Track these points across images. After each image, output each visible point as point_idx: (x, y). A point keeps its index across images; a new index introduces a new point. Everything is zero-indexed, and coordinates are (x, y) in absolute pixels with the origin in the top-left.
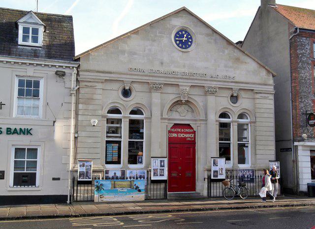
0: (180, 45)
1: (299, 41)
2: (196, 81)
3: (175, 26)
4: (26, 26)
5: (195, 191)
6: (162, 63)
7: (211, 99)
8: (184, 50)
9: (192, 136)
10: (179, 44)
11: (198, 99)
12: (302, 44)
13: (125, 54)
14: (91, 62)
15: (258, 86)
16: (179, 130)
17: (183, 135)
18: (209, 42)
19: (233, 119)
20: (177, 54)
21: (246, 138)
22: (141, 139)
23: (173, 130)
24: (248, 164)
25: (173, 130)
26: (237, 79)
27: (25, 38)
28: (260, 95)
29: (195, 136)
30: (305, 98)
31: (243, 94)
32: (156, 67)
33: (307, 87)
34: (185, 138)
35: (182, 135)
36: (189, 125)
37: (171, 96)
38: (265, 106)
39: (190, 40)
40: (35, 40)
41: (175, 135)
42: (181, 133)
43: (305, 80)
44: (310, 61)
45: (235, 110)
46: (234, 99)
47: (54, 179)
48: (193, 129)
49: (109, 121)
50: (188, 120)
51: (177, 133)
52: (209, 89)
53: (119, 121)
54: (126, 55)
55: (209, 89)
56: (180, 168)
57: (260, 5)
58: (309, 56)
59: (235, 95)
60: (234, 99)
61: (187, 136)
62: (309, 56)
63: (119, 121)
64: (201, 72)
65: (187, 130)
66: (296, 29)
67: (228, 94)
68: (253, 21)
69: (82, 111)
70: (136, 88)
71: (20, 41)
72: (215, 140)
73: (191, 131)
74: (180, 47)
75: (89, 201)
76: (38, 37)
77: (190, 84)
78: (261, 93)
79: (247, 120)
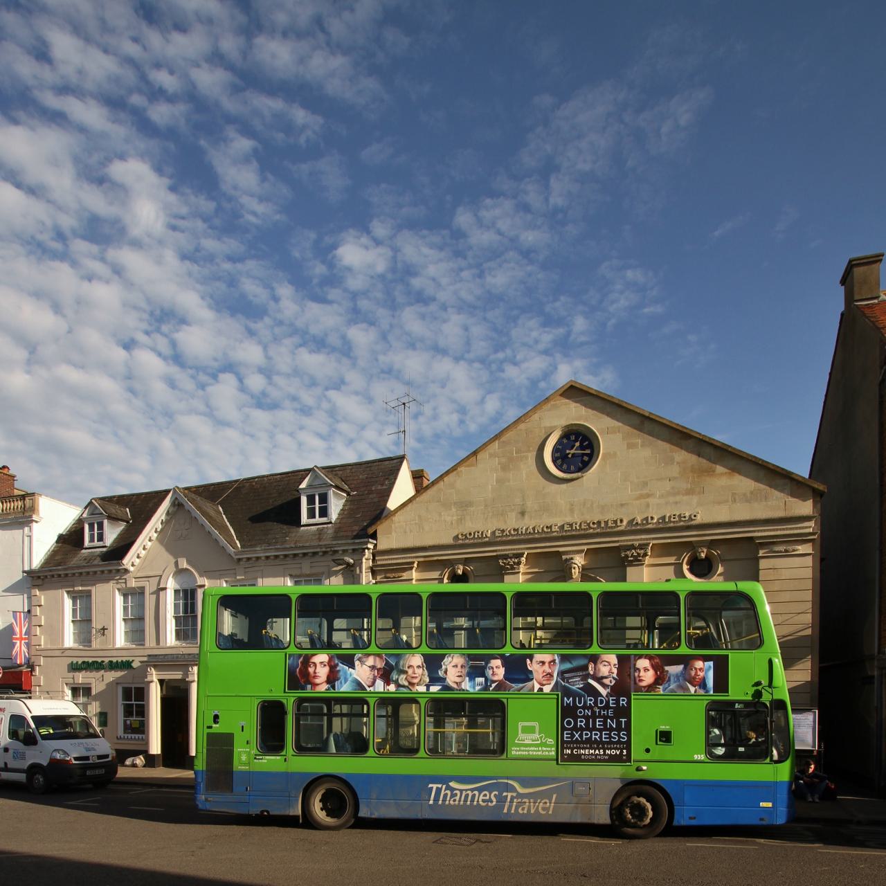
13: (451, 509)
18: (631, 446)
26: (699, 520)
27: (311, 514)
47: (243, 727)
54: (454, 510)
71: (304, 519)
74: (564, 472)
76: (308, 505)
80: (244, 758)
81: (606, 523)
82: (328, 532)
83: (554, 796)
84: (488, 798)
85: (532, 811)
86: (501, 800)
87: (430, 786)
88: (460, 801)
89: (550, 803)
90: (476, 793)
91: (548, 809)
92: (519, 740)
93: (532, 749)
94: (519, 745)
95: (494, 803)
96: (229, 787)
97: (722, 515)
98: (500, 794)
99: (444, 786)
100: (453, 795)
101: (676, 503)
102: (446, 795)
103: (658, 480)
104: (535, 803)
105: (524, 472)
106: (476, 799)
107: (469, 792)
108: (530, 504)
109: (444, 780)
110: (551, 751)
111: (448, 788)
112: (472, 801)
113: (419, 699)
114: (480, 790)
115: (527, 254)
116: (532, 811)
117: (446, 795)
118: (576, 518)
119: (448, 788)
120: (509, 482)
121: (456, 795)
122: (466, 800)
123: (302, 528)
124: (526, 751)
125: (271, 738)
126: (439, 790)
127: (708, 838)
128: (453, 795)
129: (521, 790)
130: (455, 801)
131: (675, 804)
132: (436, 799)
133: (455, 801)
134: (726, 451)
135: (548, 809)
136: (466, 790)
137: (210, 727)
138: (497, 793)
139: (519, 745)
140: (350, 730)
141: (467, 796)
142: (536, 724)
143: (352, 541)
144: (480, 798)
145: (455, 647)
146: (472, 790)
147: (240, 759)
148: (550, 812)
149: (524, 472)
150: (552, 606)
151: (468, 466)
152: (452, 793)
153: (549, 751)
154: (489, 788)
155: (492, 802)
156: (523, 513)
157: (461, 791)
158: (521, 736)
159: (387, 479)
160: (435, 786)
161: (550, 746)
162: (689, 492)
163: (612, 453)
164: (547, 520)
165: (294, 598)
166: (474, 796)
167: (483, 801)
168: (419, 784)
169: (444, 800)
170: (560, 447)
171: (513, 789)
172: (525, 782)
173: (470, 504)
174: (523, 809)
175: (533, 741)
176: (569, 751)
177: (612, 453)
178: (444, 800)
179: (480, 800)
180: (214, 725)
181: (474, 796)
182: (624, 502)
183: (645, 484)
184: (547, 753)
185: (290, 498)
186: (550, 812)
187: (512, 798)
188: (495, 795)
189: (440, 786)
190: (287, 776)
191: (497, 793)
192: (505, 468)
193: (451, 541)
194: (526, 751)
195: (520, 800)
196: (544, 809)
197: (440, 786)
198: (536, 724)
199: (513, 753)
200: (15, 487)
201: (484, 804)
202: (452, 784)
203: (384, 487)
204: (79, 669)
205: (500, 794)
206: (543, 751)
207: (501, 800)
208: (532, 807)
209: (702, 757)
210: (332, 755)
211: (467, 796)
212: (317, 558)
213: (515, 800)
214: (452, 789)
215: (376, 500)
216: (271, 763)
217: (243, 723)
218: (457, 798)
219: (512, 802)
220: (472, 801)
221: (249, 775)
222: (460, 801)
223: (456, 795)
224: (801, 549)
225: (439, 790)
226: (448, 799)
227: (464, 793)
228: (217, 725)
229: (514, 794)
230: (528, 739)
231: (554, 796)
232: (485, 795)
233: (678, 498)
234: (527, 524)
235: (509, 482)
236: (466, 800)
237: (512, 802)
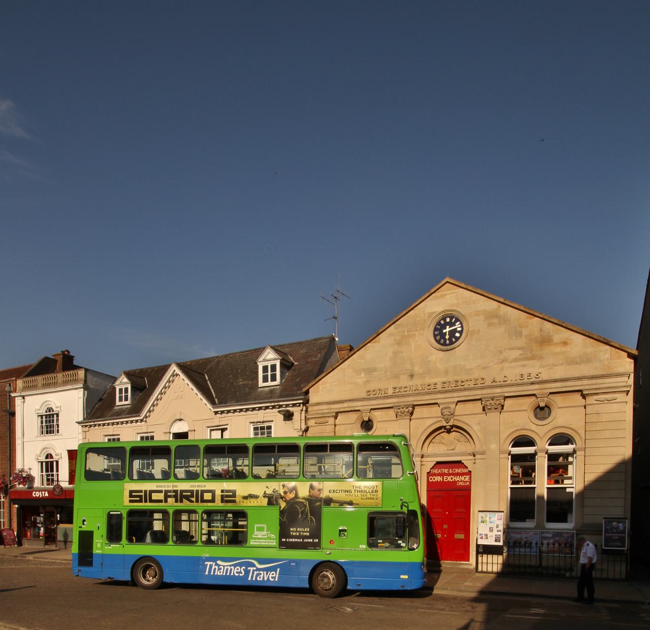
0: (438, 338)
2: (466, 393)
3: (446, 332)
4: (265, 364)
5: (469, 561)
6: (412, 376)
8: (449, 347)
9: (467, 479)
11: (470, 416)
16: (446, 471)
17: (452, 478)
18: (489, 325)
19: (543, 449)
20: (437, 357)
21: (570, 478)
22: (210, 530)
23: (436, 471)
24: (572, 522)
25: (436, 471)
26: (544, 377)
28: (595, 397)
29: (470, 478)
31: (558, 400)
32: (404, 381)
34: (455, 482)
35: (449, 479)
36: (460, 462)
37: (427, 419)
40: (274, 378)
41: (439, 479)
42: (449, 474)
45: (542, 432)
46: (542, 411)
48: (467, 467)
49: (516, 459)
50: (457, 455)
51: (442, 475)
52: (488, 403)
53: (532, 457)
54: (363, 375)
55: (488, 403)
56: (445, 526)
59: (542, 404)
60: (542, 411)
61: (457, 479)
63: (532, 457)
64: (476, 375)
65: (459, 471)
70: (377, 416)
71: (261, 384)
73: (465, 471)
76: (263, 373)
77: (456, 400)
78: (597, 394)
80: (99, 545)
81: (529, 375)
82: (277, 392)
83: (278, 570)
84: (239, 571)
85: (266, 579)
86: (247, 572)
87: (206, 563)
88: (223, 573)
89: (276, 574)
90: (233, 567)
91: (275, 578)
92: (254, 535)
93: (263, 541)
94: (255, 539)
95: (242, 575)
96: (90, 564)
97: (559, 373)
98: (247, 568)
99: (214, 564)
100: (219, 569)
101: (524, 366)
102: (215, 569)
103: (510, 349)
104: (267, 574)
105: (413, 346)
106: (232, 572)
107: (228, 567)
108: (417, 369)
109: (214, 559)
110: (273, 542)
111: (217, 564)
112: (230, 573)
113: (197, 510)
114: (235, 566)
116: (266, 579)
117: (215, 569)
118: (451, 378)
119: (217, 564)
120: (402, 353)
121: (221, 569)
122: (226, 573)
123: (259, 389)
124: (259, 542)
125: (113, 535)
126: (211, 566)
128: (219, 569)
130: (220, 572)
131: (348, 576)
132: (210, 572)
133: (220, 572)
135: (275, 578)
136: (227, 566)
137: (81, 527)
138: (244, 568)
139: (255, 539)
141: (227, 569)
142: (265, 526)
144: (235, 571)
145: (393, 477)
146: (230, 566)
147: (97, 546)
148: (276, 580)
149: (413, 346)
151: (374, 342)
153: (272, 542)
154: (240, 565)
155: (242, 573)
156: (412, 376)
157: (224, 566)
158: (256, 532)
159: (320, 352)
160: (209, 563)
161: (273, 539)
162: (533, 358)
163: (477, 330)
164: (428, 380)
165: (128, 449)
166: (231, 570)
167: (237, 573)
168: (198, 561)
169: (214, 572)
170: (439, 327)
171: (254, 566)
172: (261, 561)
173: (374, 370)
174: (260, 578)
175: (263, 536)
176: (284, 540)
177: (477, 330)
178: (214, 572)
179: (235, 572)
180: (83, 526)
181: (231, 570)
182: (485, 366)
183: (501, 352)
184: (271, 544)
186: (276, 580)
187: (254, 571)
188: (243, 569)
189: (211, 563)
190: (123, 557)
191: (244, 568)
192: (399, 343)
193: (364, 395)
194: (259, 542)
195: (258, 572)
196: (272, 578)
198: (265, 526)
199: (251, 543)
202: (219, 562)
203: (318, 359)
205: (247, 568)
206: (269, 542)
207: (247, 572)
208: (265, 575)
209: (364, 546)
210: (148, 544)
211: (227, 569)
212: (224, 415)
213: (255, 572)
214: (219, 565)
215: (310, 368)
216: (114, 549)
217: (99, 525)
218: (222, 571)
219: (253, 573)
220: (230, 573)
221: (103, 556)
222: (223, 573)
223: (221, 569)
224: (621, 397)
225: (211, 566)
226: (216, 571)
227: (226, 568)
228: (85, 526)
229: (255, 568)
230: (259, 534)
231: (278, 570)
232: (238, 569)
233: (525, 363)
234: (417, 382)
235: (402, 353)
236: (226, 573)
237: (253, 573)
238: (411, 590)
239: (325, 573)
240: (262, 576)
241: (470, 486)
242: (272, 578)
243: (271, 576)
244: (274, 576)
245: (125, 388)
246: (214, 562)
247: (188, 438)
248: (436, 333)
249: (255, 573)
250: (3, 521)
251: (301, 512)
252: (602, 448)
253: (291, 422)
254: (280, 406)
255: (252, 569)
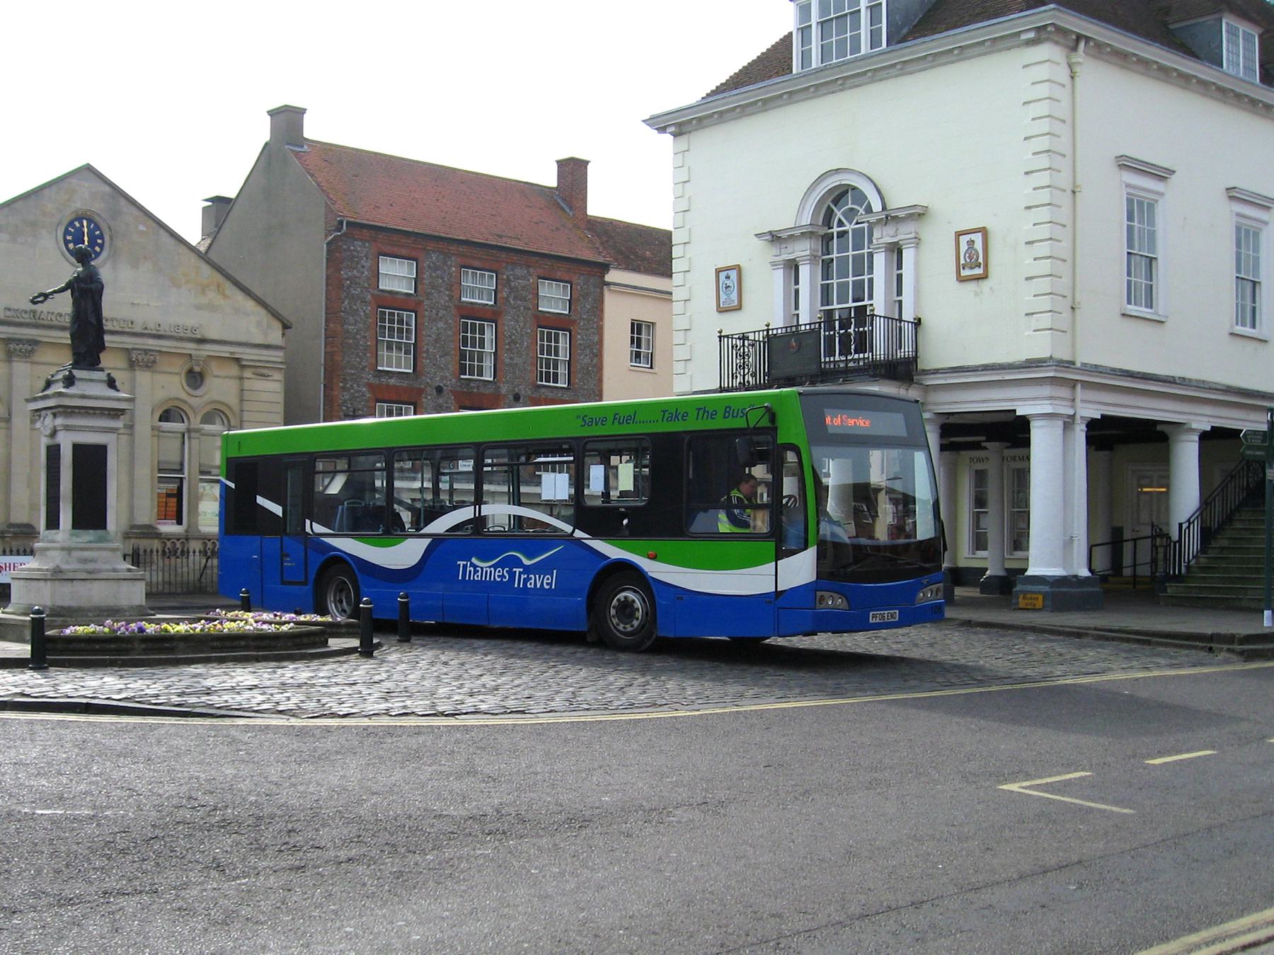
1: (345, 250)
7: (143, 377)
10: (70, 242)
12: (353, 257)
14: (218, 459)
15: (248, 350)
22: (853, 246)
30: (352, 380)
31: (215, 368)
33: (358, 354)
38: (264, 397)
39: (99, 241)
43: (354, 338)
44: (369, 297)
46: (195, 378)
57: (268, 139)
58: (366, 285)
59: (197, 369)
60: (195, 378)
62: (366, 285)
66: (341, 223)
67: (179, 366)
68: (251, 172)
69: (1145, 534)
72: (148, 472)
75: (173, 594)
79: (181, 425)
83: (555, 571)
86: (512, 575)
87: (459, 563)
100: (476, 572)
102: (470, 571)
115: (1178, 578)
127: (792, 673)
128: (476, 572)
129: (526, 562)
134: (118, 192)
140: (124, 370)
141: (486, 571)
143: (1088, 632)
146: (490, 567)
150: (409, 373)
152: (475, 569)
166: (491, 572)
174: (531, 584)
185: (1022, 567)
189: (465, 563)
196: (547, 584)
197: (465, 563)
200: (903, 319)
201: (499, 580)
204: (191, 594)
211: (486, 571)
214: (475, 566)
218: (479, 574)
219: (520, 577)
231: (555, 571)
232: (499, 572)
237: (520, 577)
238: (842, 652)
239: (621, 596)
240: (533, 581)
241: (686, 536)
242: (547, 584)
243: (545, 581)
244: (550, 581)
245: (80, 451)
246: (468, 561)
247: (668, 235)
248: (69, 238)
249: (523, 577)
250: (1139, 229)
251: (1245, 274)
252: (356, 473)
253: (162, 458)
254: (805, 39)
255: (518, 570)
